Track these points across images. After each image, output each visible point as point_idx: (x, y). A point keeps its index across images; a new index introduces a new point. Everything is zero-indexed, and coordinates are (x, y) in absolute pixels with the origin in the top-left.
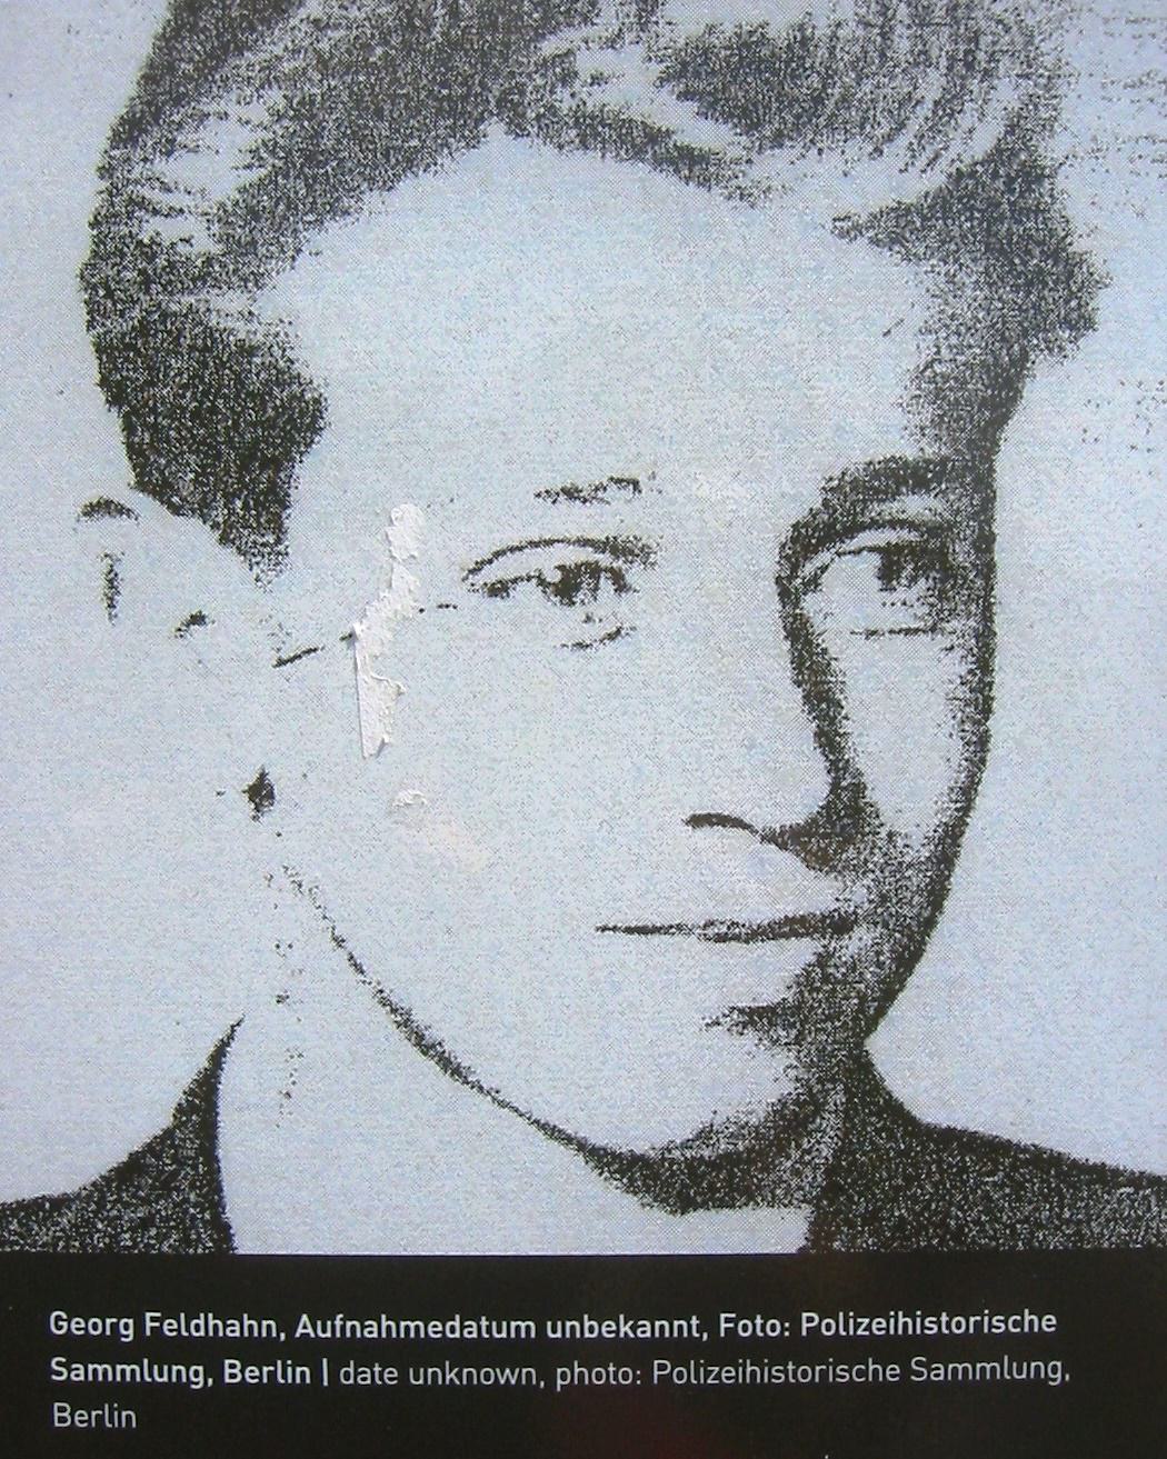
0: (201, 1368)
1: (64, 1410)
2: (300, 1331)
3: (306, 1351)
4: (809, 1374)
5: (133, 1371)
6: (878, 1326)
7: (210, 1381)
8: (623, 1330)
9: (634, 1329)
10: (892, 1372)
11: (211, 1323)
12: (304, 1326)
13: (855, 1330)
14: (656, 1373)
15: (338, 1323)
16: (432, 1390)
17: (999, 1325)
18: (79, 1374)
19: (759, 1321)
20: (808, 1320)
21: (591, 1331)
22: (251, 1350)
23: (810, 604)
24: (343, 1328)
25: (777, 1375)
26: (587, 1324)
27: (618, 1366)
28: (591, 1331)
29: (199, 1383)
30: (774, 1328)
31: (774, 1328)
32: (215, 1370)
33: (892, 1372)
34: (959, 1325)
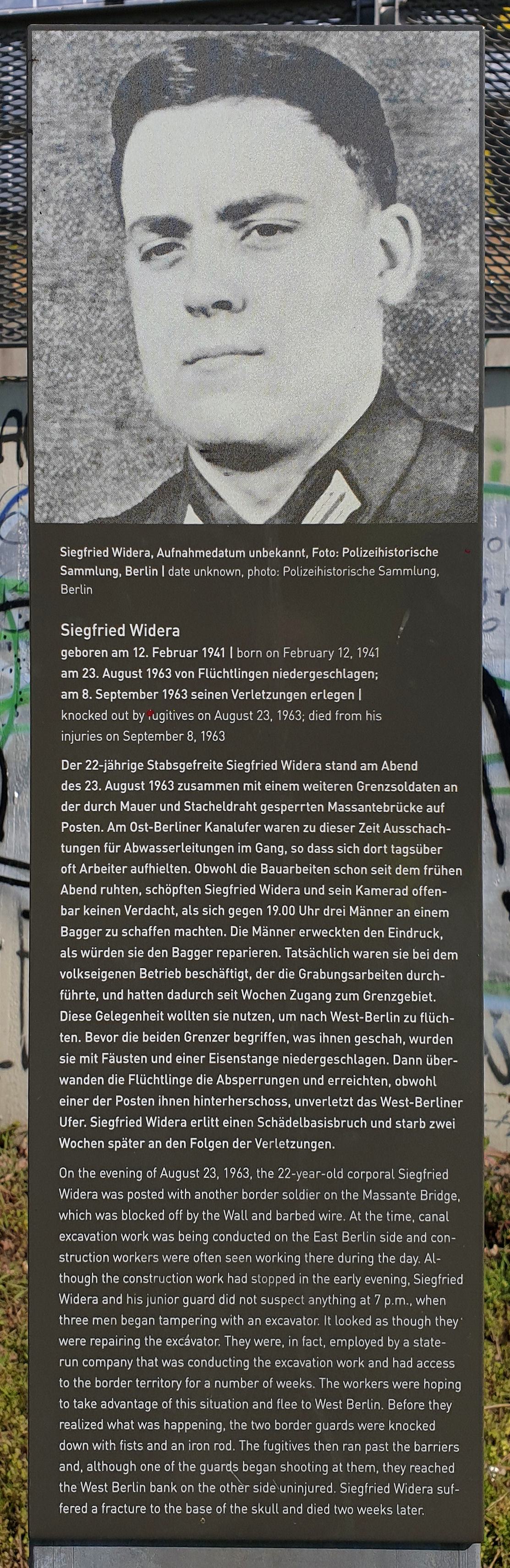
0: (282, 847)
1: (116, 1485)
3: (156, 563)
4: (341, 572)
5: (136, 695)
6: (371, 553)
7: (286, 852)
10: (372, 572)
12: (160, 553)
14: (284, 572)
15: (173, 551)
16: (203, 577)
17: (416, 553)
18: (71, 572)
20: (345, 551)
22: (136, 563)
24: (175, 553)
25: (331, 572)
26: (264, 552)
29: (282, 853)
30: (333, 554)
31: (333, 554)
32: (122, 571)
33: (372, 572)
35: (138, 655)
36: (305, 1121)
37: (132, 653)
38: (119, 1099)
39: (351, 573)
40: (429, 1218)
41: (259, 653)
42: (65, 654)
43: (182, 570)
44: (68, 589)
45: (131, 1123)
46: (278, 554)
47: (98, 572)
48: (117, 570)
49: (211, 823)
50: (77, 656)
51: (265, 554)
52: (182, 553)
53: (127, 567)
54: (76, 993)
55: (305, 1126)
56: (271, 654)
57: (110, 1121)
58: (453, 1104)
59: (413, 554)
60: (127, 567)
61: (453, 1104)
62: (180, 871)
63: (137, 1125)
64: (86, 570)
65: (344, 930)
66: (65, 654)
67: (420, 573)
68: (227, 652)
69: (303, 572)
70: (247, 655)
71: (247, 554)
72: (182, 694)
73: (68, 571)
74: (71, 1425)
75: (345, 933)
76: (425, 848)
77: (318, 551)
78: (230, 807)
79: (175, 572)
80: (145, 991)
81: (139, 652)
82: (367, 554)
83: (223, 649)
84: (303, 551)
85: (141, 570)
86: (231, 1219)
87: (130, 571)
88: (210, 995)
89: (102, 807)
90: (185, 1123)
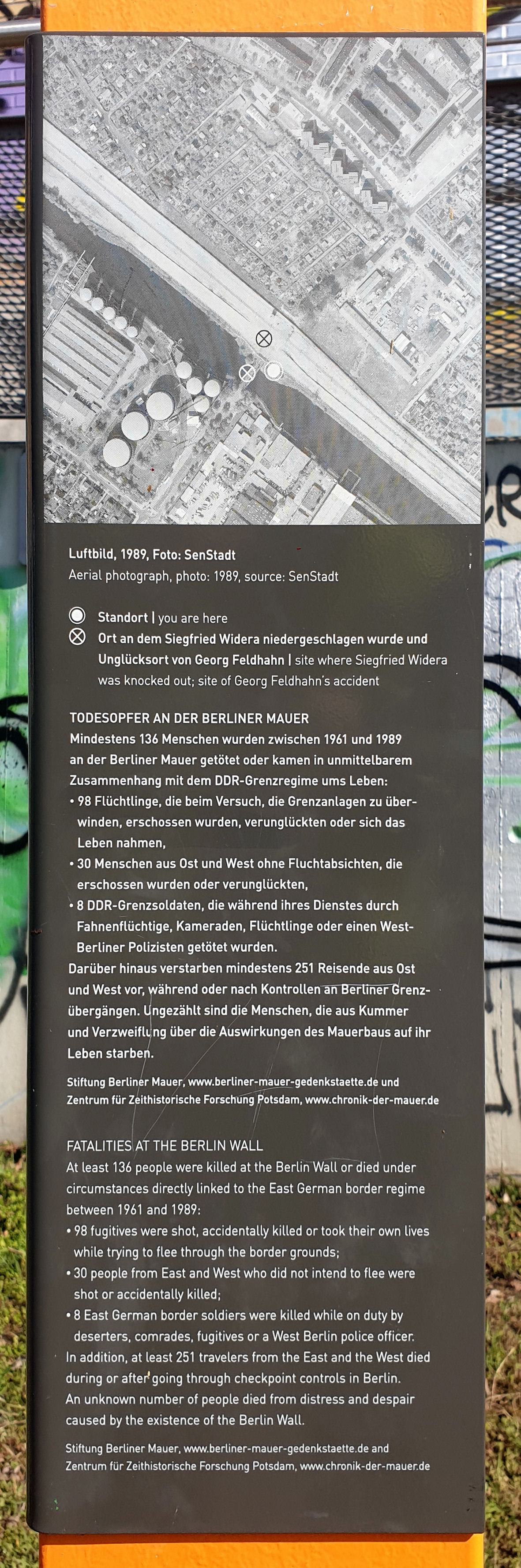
2: (155, 720)
8: (263, 1380)
9: (278, 761)
11: (259, 659)
12: (100, 1253)
13: (150, 949)
19: (169, 553)
21: (169, 1401)
23: (197, 417)
27: (130, 572)
28: (169, 1401)
34: (168, 1101)
38: (132, 945)
45: (205, 640)
49: (183, 922)
57: (184, 638)
62: (136, 887)
63: (211, 642)
78: (253, 661)
86: (321, 1170)
88: (254, 989)
89: (384, 906)
90: (258, 640)
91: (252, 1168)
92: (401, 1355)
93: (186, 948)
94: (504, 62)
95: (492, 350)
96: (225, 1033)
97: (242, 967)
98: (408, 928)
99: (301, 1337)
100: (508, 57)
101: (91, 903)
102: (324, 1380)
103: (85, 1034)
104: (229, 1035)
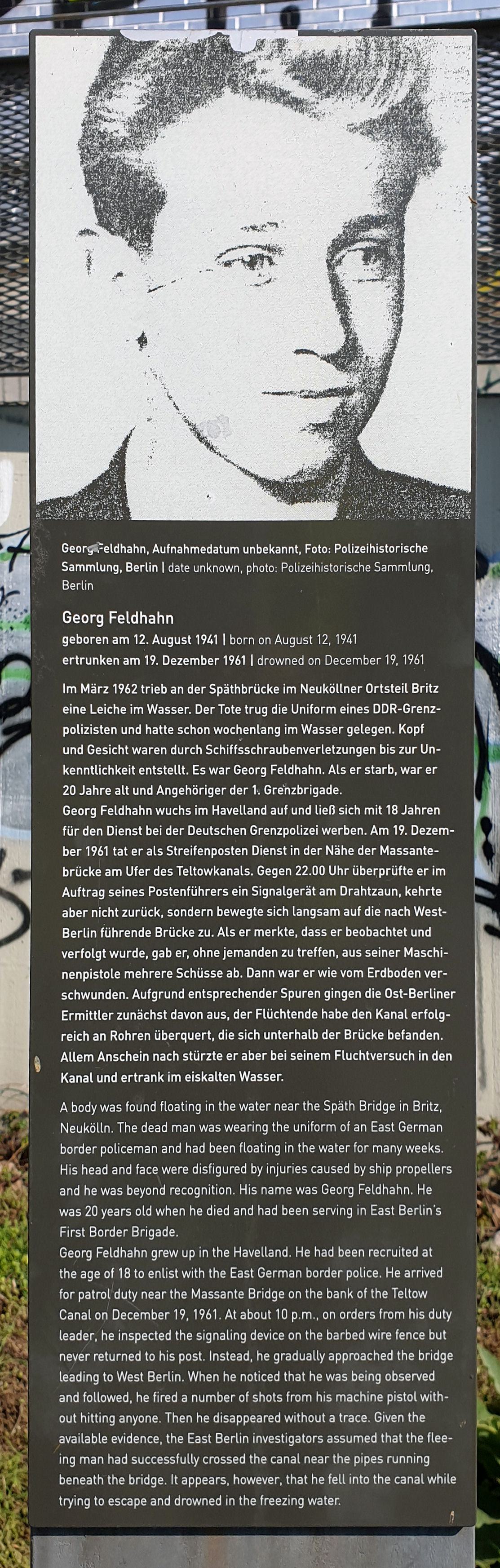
3: (156, 559)
4: (338, 568)
12: (156, 549)
14: (282, 568)
15: (168, 548)
16: (202, 574)
18: (72, 568)
20: (337, 547)
22: (137, 559)
24: (170, 549)
26: (258, 548)
30: (325, 550)
31: (325, 550)
32: (122, 567)
35: (139, 642)
36: (313, 1033)
37: (132, 639)
39: (347, 569)
40: (280, 1461)
41: (251, 640)
42: (66, 641)
43: (182, 566)
44: (69, 585)
46: (271, 550)
47: (99, 569)
48: (117, 566)
50: (78, 642)
51: (259, 550)
52: (177, 549)
53: (127, 563)
54: (116, 931)
55: (314, 1038)
56: (264, 641)
58: (446, 995)
59: (404, 550)
60: (127, 563)
61: (446, 995)
64: (87, 566)
65: (286, 930)
66: (66, 641)
67: (414, 569)
68: (220, 639)
69: (301, 568)
70: (239, 642)
71: (241, 550)
72: (132, 689)
73: (69, 567)
74: (240, 1127)
75: (288, 932)
76: (163, 1034)
77: (311, 547)
79: (174, 568)
80: (163, 726)
81: (140, 639)
82: (359, 550)
83: (216, 636)
84: (296, 547)
85: (141, 566)
87: (131, 567)
89: (188, 751)
91: (404, 1439)
92: (176, 1271)
93: (322, 994)
94: (341, 18)
95: (18, 296)
96: (68, 894)
97: (336, 992)
98: (442, 913)
99: (213, 1439)
100: (345, 12)
101: (110, 829)
102: (95, 1296)
103: (114, 1079)
104: (72, 896)
